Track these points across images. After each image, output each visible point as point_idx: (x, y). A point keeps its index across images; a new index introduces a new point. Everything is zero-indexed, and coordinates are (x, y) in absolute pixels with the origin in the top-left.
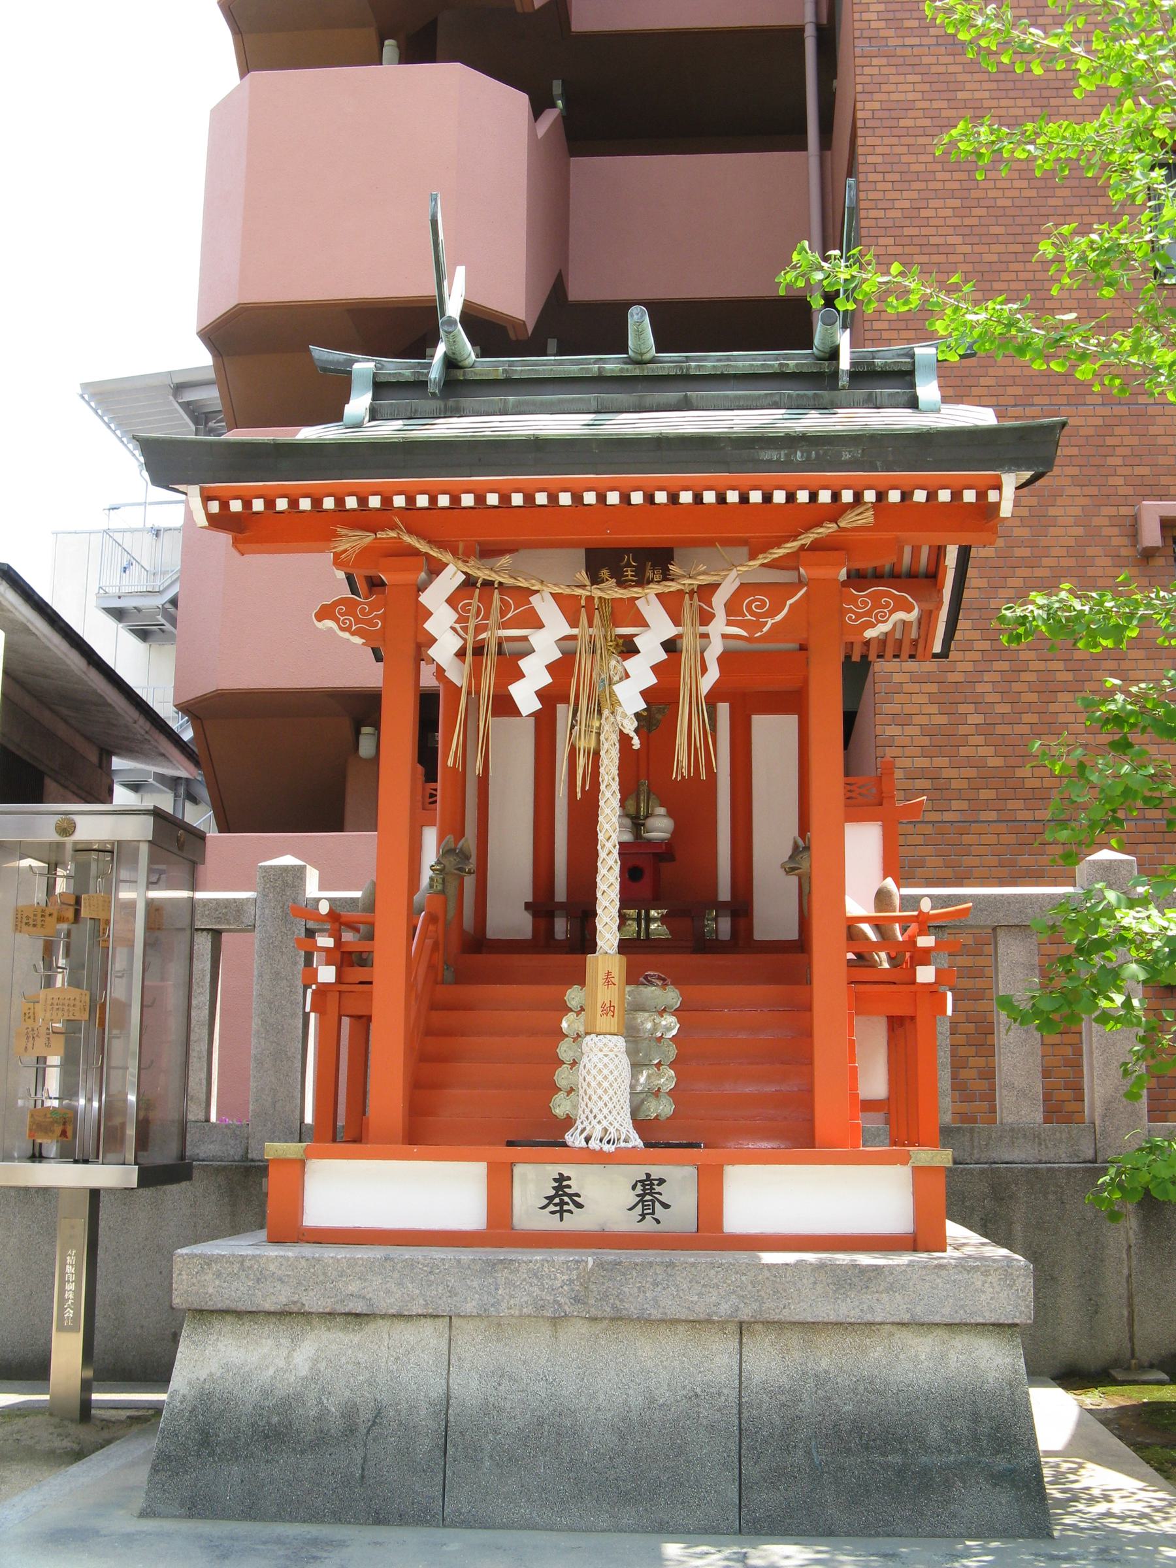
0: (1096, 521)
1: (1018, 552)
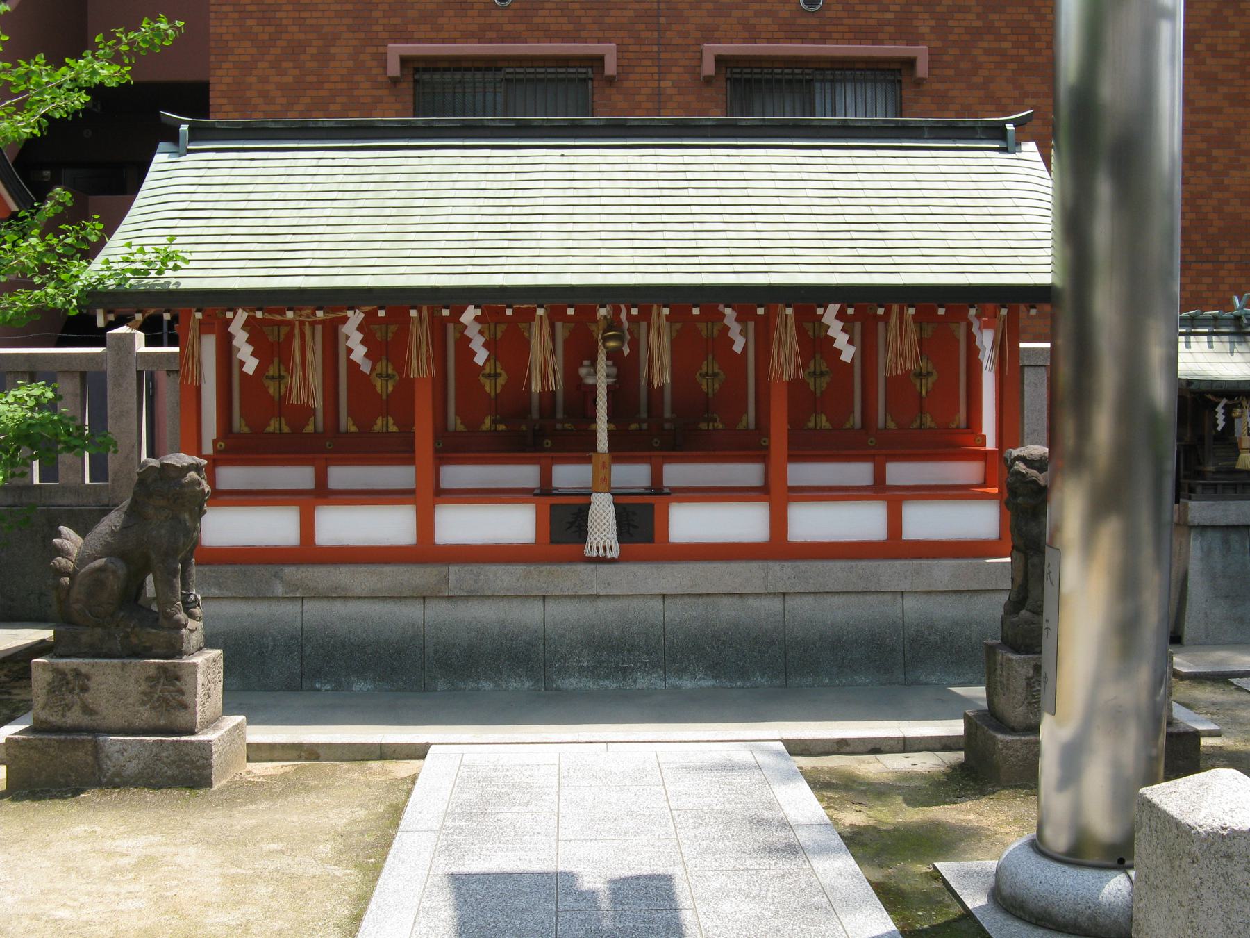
0: (362, 57)
1: (309, 79)
